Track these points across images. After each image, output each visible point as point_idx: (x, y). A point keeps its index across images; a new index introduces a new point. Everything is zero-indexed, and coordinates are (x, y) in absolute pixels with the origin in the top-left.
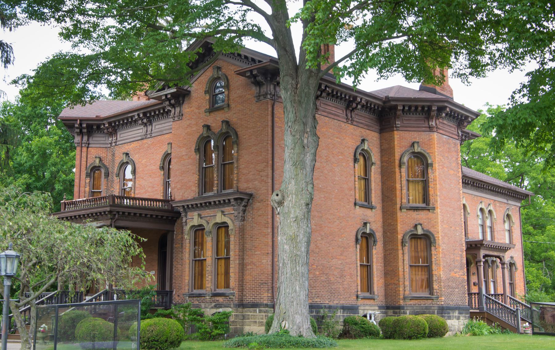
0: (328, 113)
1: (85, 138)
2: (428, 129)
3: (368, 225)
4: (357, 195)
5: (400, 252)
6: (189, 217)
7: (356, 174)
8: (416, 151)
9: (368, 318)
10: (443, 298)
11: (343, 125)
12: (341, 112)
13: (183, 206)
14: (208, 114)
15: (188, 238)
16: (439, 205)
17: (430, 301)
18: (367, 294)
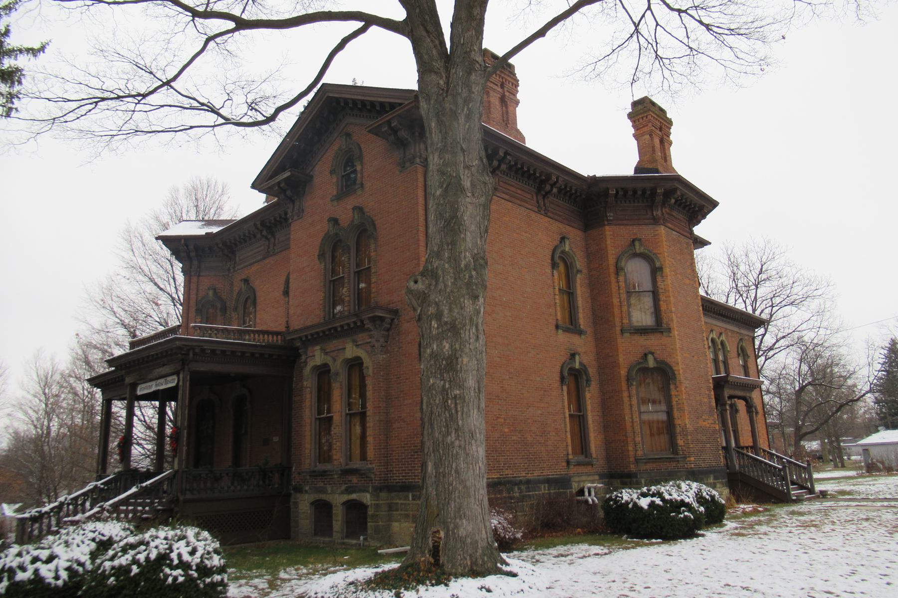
0: (511, 196)
1: (195, 262)
2: (652, 221)
3: (577, 357)
4: (559, 314)
5: (625, 394)
6: (310, 354)
7: (556, 284)
8: (638, 251)
9: (587, 493)
10: (692, 459)
11: (533, 215)
12: (529, 196)
13: (300, 338)
14: (335, 203)
15: (308, 384)
16: (674, 325)
17: (674, 464)
18: (582, 458)
